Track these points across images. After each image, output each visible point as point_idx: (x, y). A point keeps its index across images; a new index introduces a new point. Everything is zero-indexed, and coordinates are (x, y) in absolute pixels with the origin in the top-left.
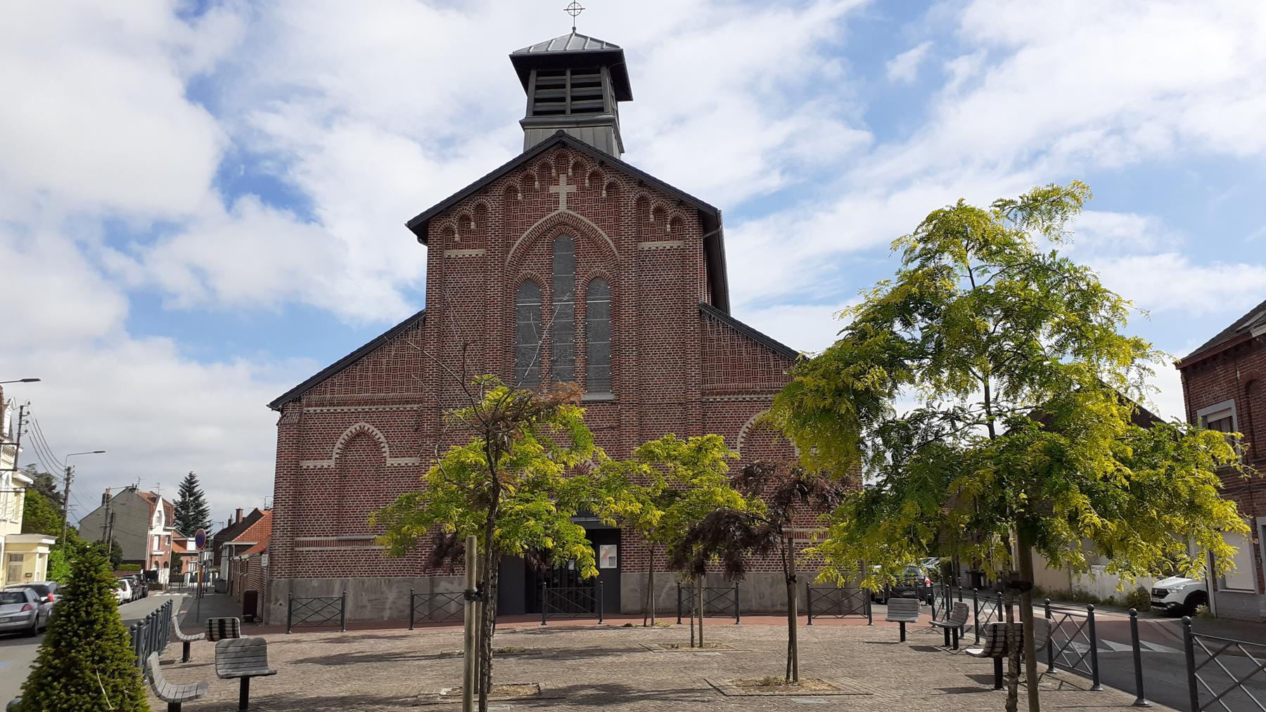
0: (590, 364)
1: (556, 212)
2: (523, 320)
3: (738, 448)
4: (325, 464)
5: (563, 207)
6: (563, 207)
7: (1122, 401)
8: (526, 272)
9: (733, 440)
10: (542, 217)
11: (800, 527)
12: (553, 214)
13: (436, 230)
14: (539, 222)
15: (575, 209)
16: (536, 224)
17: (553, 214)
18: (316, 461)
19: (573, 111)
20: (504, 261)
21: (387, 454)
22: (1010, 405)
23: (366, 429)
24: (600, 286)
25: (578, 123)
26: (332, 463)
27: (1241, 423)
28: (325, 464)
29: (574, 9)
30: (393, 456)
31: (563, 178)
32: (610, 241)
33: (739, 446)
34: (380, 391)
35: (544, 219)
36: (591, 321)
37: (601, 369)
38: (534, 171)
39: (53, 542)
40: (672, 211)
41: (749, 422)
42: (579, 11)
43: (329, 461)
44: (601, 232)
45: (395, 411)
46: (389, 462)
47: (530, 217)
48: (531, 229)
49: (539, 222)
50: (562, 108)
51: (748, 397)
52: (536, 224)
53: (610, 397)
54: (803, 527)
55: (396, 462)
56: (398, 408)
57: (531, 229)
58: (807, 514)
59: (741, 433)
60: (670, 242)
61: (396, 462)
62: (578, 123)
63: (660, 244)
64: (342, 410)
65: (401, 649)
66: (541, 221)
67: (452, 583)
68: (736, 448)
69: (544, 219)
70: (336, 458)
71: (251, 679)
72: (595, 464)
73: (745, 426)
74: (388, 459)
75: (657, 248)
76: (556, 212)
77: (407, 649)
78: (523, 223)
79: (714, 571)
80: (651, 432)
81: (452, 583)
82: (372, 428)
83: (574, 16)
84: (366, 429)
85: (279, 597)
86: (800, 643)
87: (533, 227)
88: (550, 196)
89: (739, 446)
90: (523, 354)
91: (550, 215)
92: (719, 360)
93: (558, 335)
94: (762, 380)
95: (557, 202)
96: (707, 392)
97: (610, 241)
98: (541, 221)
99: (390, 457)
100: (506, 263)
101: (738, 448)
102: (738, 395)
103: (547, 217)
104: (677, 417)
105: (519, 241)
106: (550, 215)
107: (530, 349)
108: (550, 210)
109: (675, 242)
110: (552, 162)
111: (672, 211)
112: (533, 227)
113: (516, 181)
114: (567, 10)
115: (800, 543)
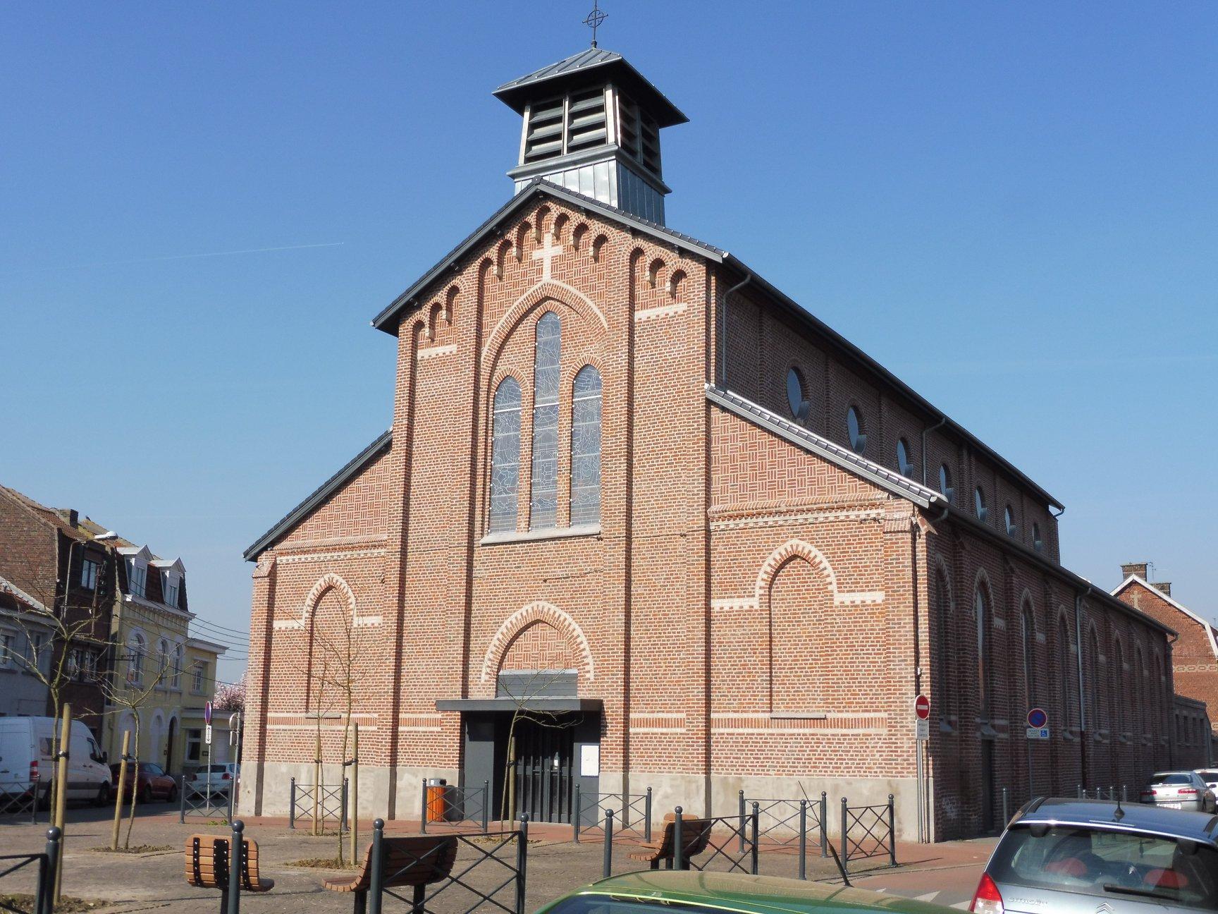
1: (539, 284)
2: (502, 432)
3: (757, 595)
4: (746, 603)
5: (547, 277)
6: (547, 277)
8: (505, 367)
9: (750, 585)
10: (523, 292)
11: (838, 711)
12: (536, 287)
14: (519, 301)
15: (561, 277)
16: (516, 303)
17: (536, 287)
18: (853, 594)
19: (572, 149)
21: (834, 587)
24: (590, 377)
25: (575, 163)
26: (755, 603)
27: (987, 640)
28: (746, 603)
32: (600, 315)
33: (758, 592)
34: (349, 533)
35: (526, 295)
36: (579, 427)
40: (673, 262)
41: (772, 556)
42: (600, 19)
43: (751, 599)
46: (838, 598)
47: (510, 294)
48: (510, 311)
49: (519, 301)
50: (556, 149)
51: (771, 520)
52: (516, 303)
54: (842, 711)
55: (847, 598)
56: (366, 554)
57: (510, 311)
58: (848, 691)
60: (675, 306)
61: (847, 598)
62: (575, 163)
64: (313, 558)
66: (521, 299)
67: (416, 776)
68: (753, 596)
69: (526, 295)
70: (760, 595)
71: (384, 836)
72: (577, 622)
73: (766, 563)
74: (356, 619)
75: (658, 316)
76: (539, 284)
78: (501, 305)
79: (721, 773)
80: (645, 576)
81: (416, 776)
85: (247, 783)
87: (513, 307)
88: (533, 263)
89: (758, 592)
90: (501, 477)
91: (532, 290)
92: (734, 468)
93: (540, 448)
94: (791, 495)
95: (540, 271)
96: (716, 516)
97: (600, 315)
98: (521, 299)
101: (757, 595)
102: (729, 520)
103: (529, 292)
104: (678, 554)
105: (497, 328)
106: (532, 290)
107: (509, 470)
108: (532, 282)
109: (680, 305)
111: (673, 262)
112: (513, 307)
115: (849, 735)
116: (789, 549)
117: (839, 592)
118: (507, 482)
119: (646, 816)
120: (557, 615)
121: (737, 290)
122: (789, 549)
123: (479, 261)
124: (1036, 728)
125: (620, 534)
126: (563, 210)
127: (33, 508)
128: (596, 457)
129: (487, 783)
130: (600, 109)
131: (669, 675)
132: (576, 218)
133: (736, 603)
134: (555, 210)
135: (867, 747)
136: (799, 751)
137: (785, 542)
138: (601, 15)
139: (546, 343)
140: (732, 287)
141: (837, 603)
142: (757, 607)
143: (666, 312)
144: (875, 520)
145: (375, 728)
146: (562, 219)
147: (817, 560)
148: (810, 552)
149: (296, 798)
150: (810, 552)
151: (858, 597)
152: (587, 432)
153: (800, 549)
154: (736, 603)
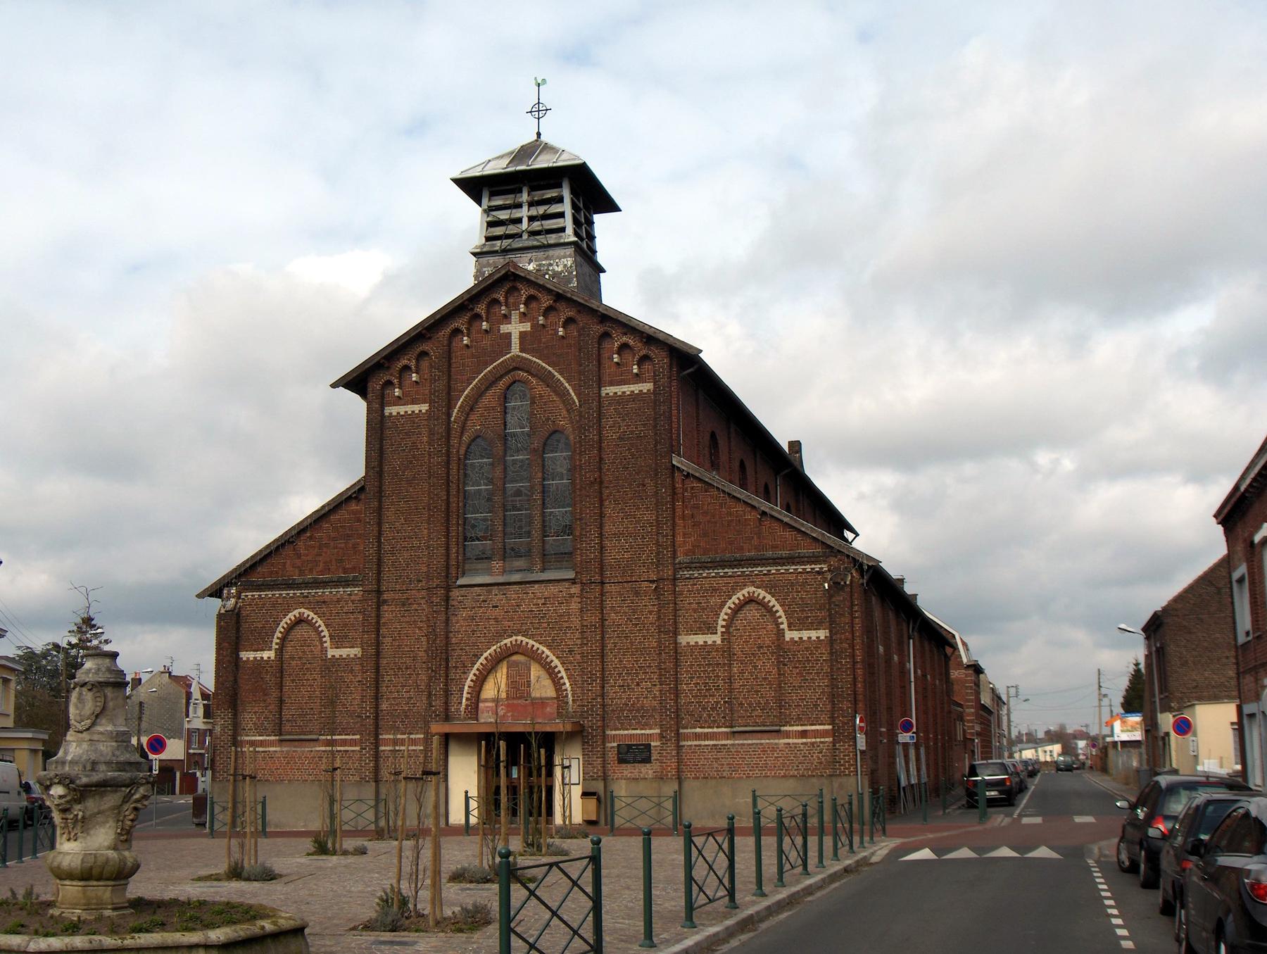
0: (548, 536)
4: (710, 639)
7: (848, 556)
13: (375, 385)
20: (449, 415)
21: (785, 626)
22: (321, 564)
23: (305, 616)
26: (717, 639)
28: (710, 639)
29: (539, 111)
30: (790, 627)
31: (515, 316)
33: (720, 630)
37: (561, 542)
38: (481, 309)
39: (46, 737)
42: (534, 110)
44: (559, 377)
45: (270, 598)
53: (571, 575)
55: (795, 635)
59: (722, 614)
61: (795, 635)
63: (627, 389)
65: (198, 885)
68: (716, 633)
70: (722, 632)
74: (329, 650)
77: (85, 905)
82: (312, 615)
83: (539, 119)
84: (305, 616)
86: (607, 912)
99: (331, 648)
100: (452, 419)
110: (501, 298)
113: (460, 323)
114: (531, 112)
116: (747, 595)
117: (789, 630)
118: (479, 531)
119: (262, 815)
120: (535, 648)
121: (688, 374)
122: (747, 595)
123: (448, 330)
124: (905, 734)
125: (596, 579)
126: (532, 292)
127: (1159, 658)
128: (566, 511)
129: (851, 796)
130: (560, 200)
131: (387, 682)
132: (546, 301)
133: (700, 639)
134: (525, 293)
135: (814, 753)
136: (757, 758)
137: (743, 589)
138: (544, 108)
139: (514, 408)
140: (684, 371)
141: (787, 639)
142: (719, 642)
143: (632, 389)
144: (818, 572)
145: (358, 748)
146: (531, 299)
147: (771, 604)
148: (764, 598)
149: (215, 813)
150: (764, 598)
151: (805, 635)
152: (557, 489)
153: (756, 595)
154: (700, 639)
